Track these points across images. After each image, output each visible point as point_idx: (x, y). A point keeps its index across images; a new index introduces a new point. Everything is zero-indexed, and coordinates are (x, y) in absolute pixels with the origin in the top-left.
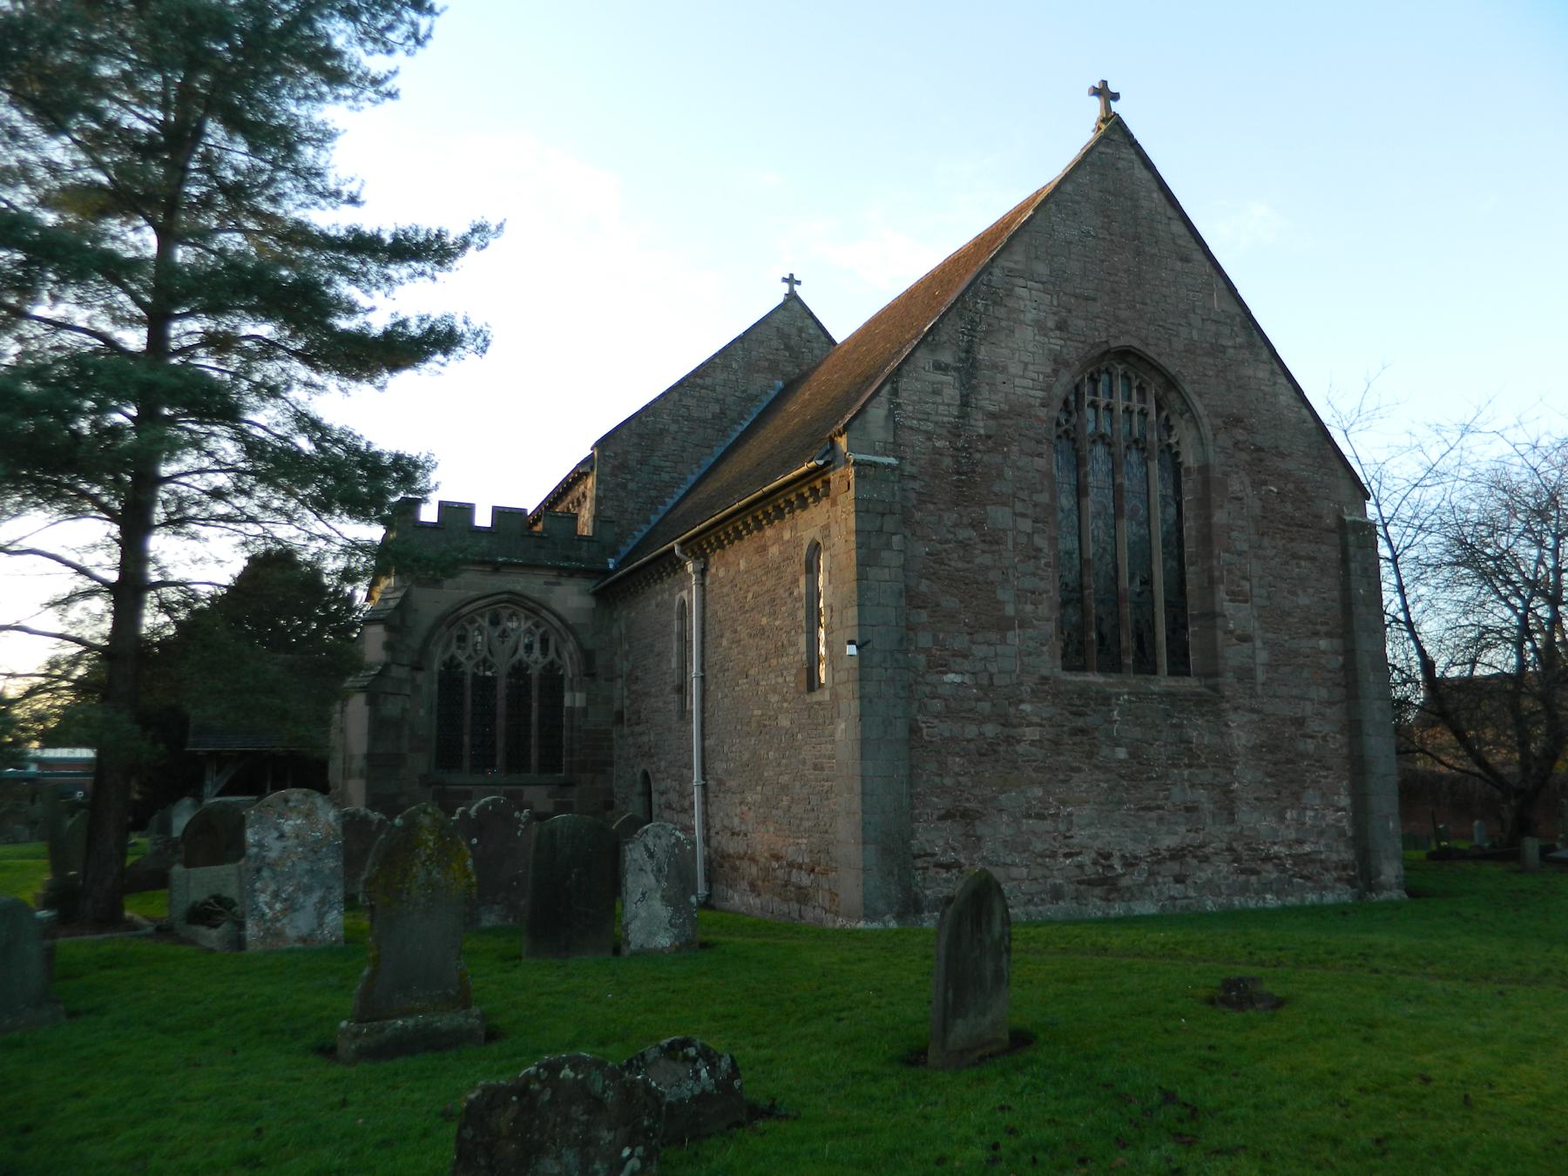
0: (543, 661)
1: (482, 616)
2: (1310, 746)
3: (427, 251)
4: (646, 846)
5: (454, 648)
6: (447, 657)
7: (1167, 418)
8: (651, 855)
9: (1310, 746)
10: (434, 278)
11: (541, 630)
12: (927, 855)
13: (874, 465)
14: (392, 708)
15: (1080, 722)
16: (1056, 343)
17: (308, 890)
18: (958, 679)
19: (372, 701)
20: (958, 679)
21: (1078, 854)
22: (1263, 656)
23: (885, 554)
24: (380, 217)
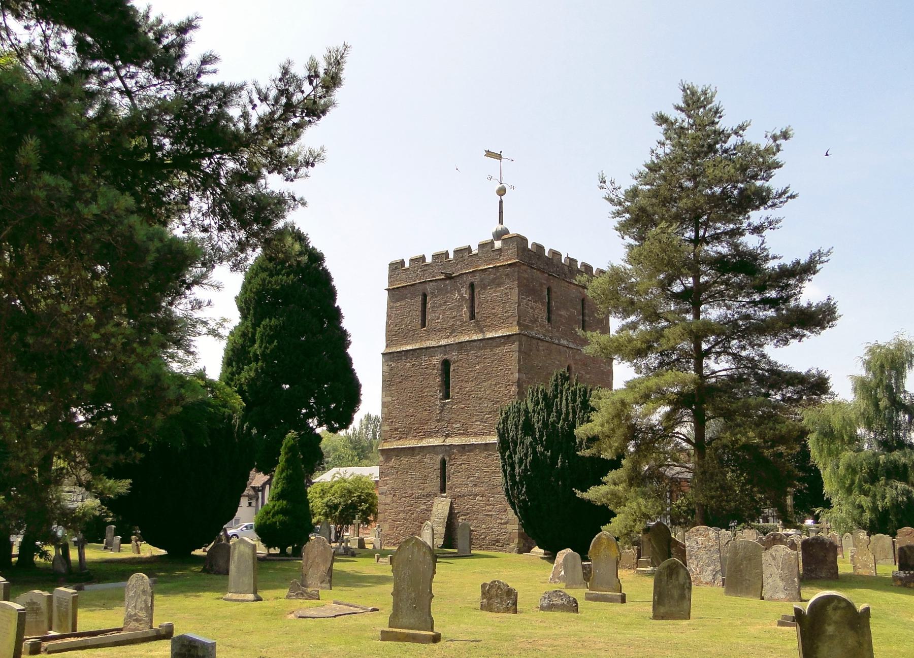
8: (774, 559)
10: (810, 280)
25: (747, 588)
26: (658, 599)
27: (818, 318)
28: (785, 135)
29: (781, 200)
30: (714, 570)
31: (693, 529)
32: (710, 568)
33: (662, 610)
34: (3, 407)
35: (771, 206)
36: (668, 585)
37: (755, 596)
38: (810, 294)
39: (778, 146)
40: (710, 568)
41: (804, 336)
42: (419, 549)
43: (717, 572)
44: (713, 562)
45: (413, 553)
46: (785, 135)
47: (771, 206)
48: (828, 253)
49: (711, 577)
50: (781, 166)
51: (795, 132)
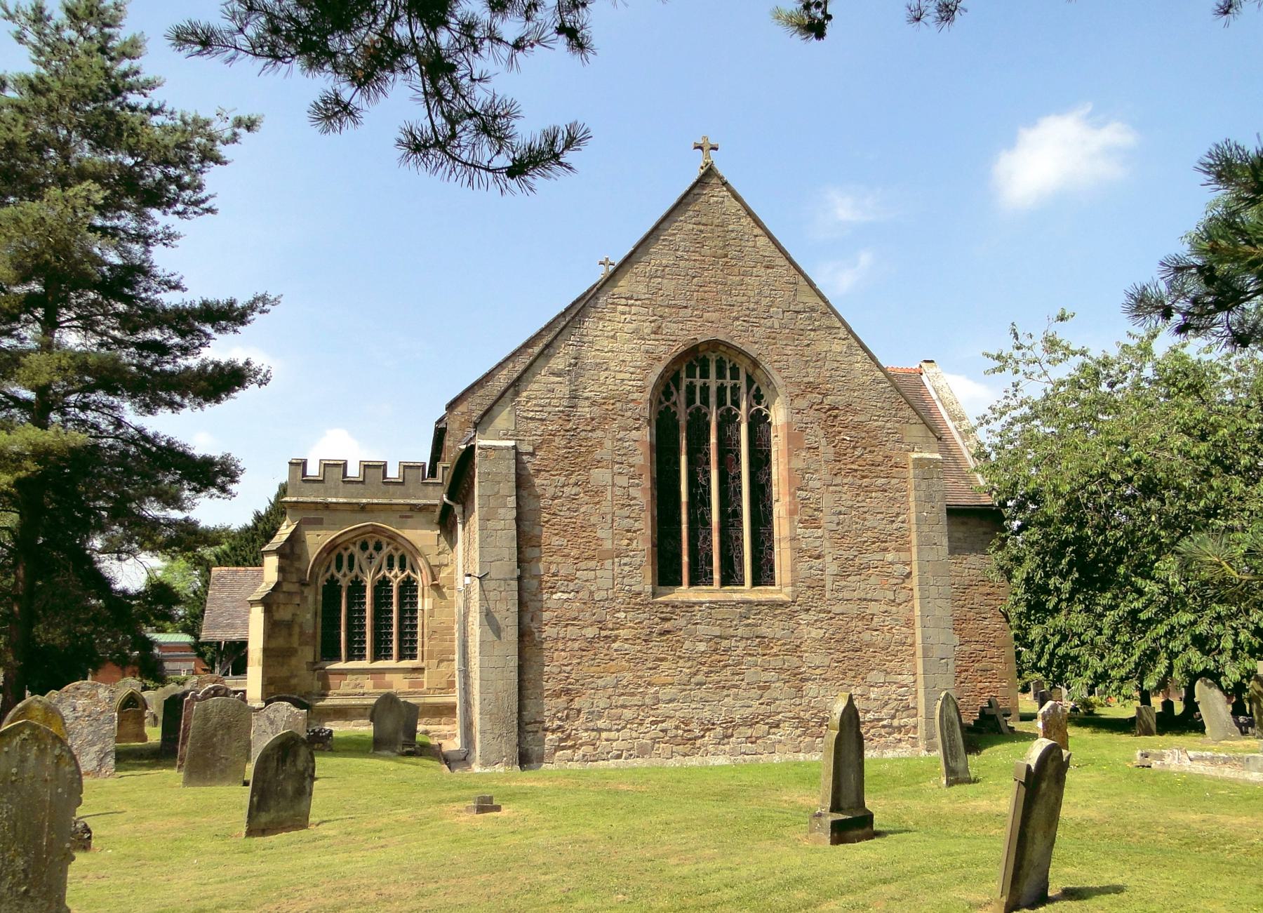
0: (402, 576)
1: (354, 544)
2: (877, 637)
3: (227, 316)
4: (268, 717)
5: (333, 569)
6: (328, 575)
7: (758, 389)
8: (272, 723)
9: (877, 637)
10: (235, 331)
11: (400, 553)
12: (536, 722)
13: (494, 448)
14: (284, 614)
15: (667, 626)
16: (650, 344)
17: (92, 744)
18: (565, 596)
19: (268, 612)
20: (565, 596)
21: (663, 722)
22: (832, 568)
23: (502, 511)
24: (191, 297)
25: (222, 771)
26: (259, 802)
27: (222, 382)
28: (250, 125)
29: (196, 209)
30: (101, 751)
31: (70, 687)
32: (96, 748)
33: (264, 818)
34: (11, 94)
35: (178, 213)
36: (277, 774)
37: (235, 782)
38: (221, 349)
39: (235, 134)
40: (96, 748)
41: (182, 406)
42: (42, 751)
43: (106, 754)
44: (102, 738)
45: (23, 760)
46: (250, 125)
47: (178, 213)
48: (275, 302)
49: (95, 763)
50: (226, 163)
51: (263, 128)
